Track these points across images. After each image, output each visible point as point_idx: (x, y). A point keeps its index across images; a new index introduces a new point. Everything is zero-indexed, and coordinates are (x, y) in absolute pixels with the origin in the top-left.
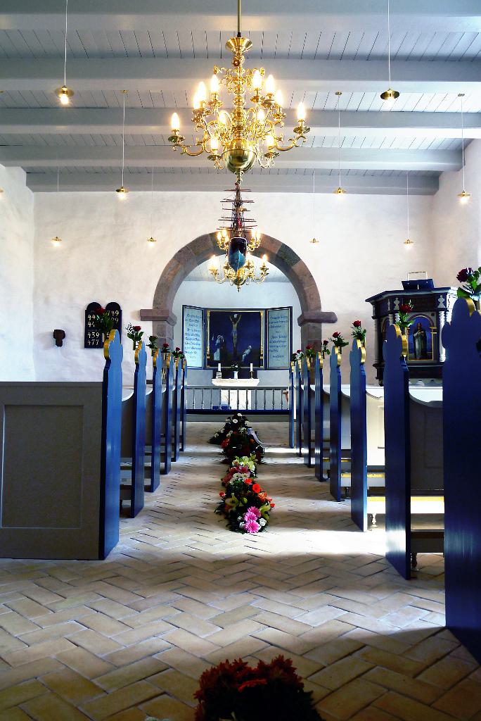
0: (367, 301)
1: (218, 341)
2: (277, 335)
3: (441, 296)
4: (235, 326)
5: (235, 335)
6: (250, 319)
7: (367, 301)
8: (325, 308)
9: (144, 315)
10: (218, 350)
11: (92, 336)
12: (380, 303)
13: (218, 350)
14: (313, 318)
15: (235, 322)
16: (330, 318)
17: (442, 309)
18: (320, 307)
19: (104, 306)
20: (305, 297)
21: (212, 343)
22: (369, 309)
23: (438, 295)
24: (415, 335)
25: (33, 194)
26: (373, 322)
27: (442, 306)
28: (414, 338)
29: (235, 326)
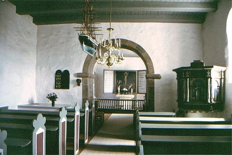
0: (173, 70)
1: (119, 83)
2: (141, 80)
3: (208, 71)
4: (126, 77)
5: (126, 80)
6: (132, 74)
7: (173, 70)
8: (156, 72)
9: (78, 75)
10: (119, 86)
11: (59, 83)
12: (179, 71)
13: (119, 86)
14: (151, 78)
15: (126, 76)
16: (158, 77)
17: (209, 77)
18: (154, 72)
19: (62, 71)
20: (147, 66)
21: (117, 83)
22: (175, 74)
23: (207, 71)
24: (196, 89)
25: (35, 27)
26: (176, 81)
27: (208, 76)
28: (195, 90)
29: (126, 77)
